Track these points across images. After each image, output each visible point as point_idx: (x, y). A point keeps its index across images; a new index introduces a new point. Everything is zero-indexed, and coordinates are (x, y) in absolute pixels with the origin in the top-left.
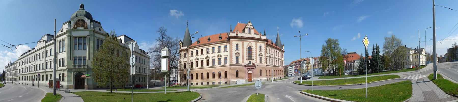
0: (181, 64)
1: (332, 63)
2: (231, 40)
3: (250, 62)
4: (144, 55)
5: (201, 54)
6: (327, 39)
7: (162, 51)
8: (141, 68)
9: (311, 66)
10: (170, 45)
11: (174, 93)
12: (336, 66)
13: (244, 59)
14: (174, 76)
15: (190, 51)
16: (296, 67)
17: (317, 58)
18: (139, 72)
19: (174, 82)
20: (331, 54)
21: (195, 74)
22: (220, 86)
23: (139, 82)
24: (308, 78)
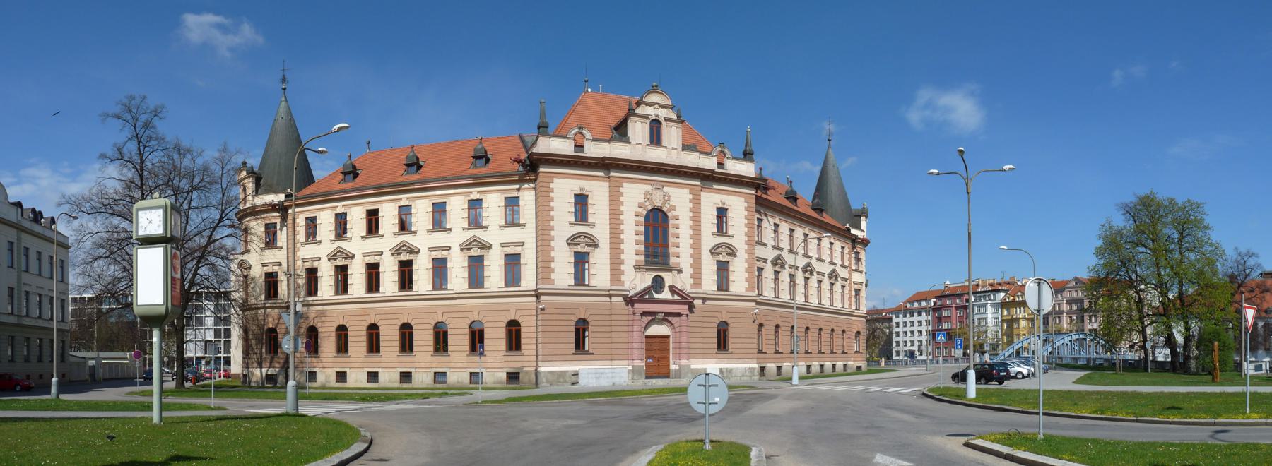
0: (246, 277)
1: (1164, 313)
2: (541, 170)
3: (658, 284)
4: (36, 228)
5: (364, 233)
6: (1130, 198)
7: (138, 210)
8: (23, 294)
9: (1032, 320)
10: (184, 181)
11: (209, 420)
12: (1188, 329)
13: (623, 267)
14: (210, 336)
15: (301, 216)
16: (940, 319)
17: (1068, 282)
18: (12, 314)
19: (208, 363)
20: (1158, 268)
21: (334, 329)
22: (479, 395)
23: (12, 360)
24: (1015, 377)
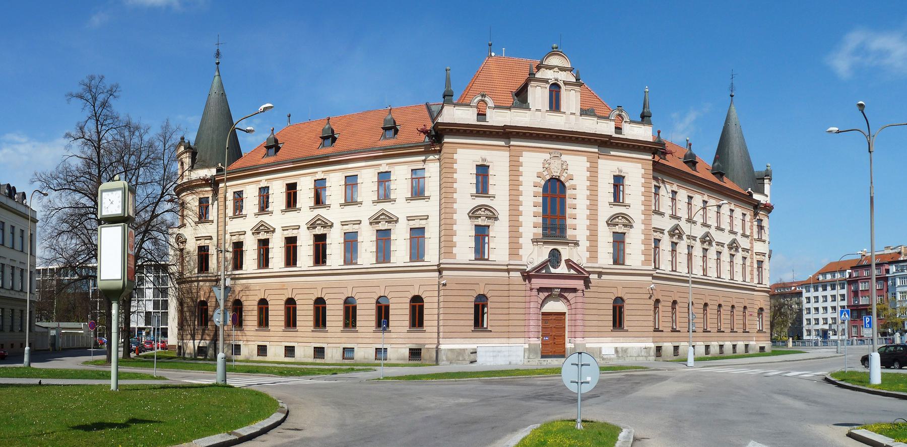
3: (555, 257)
13: (521, 241)
